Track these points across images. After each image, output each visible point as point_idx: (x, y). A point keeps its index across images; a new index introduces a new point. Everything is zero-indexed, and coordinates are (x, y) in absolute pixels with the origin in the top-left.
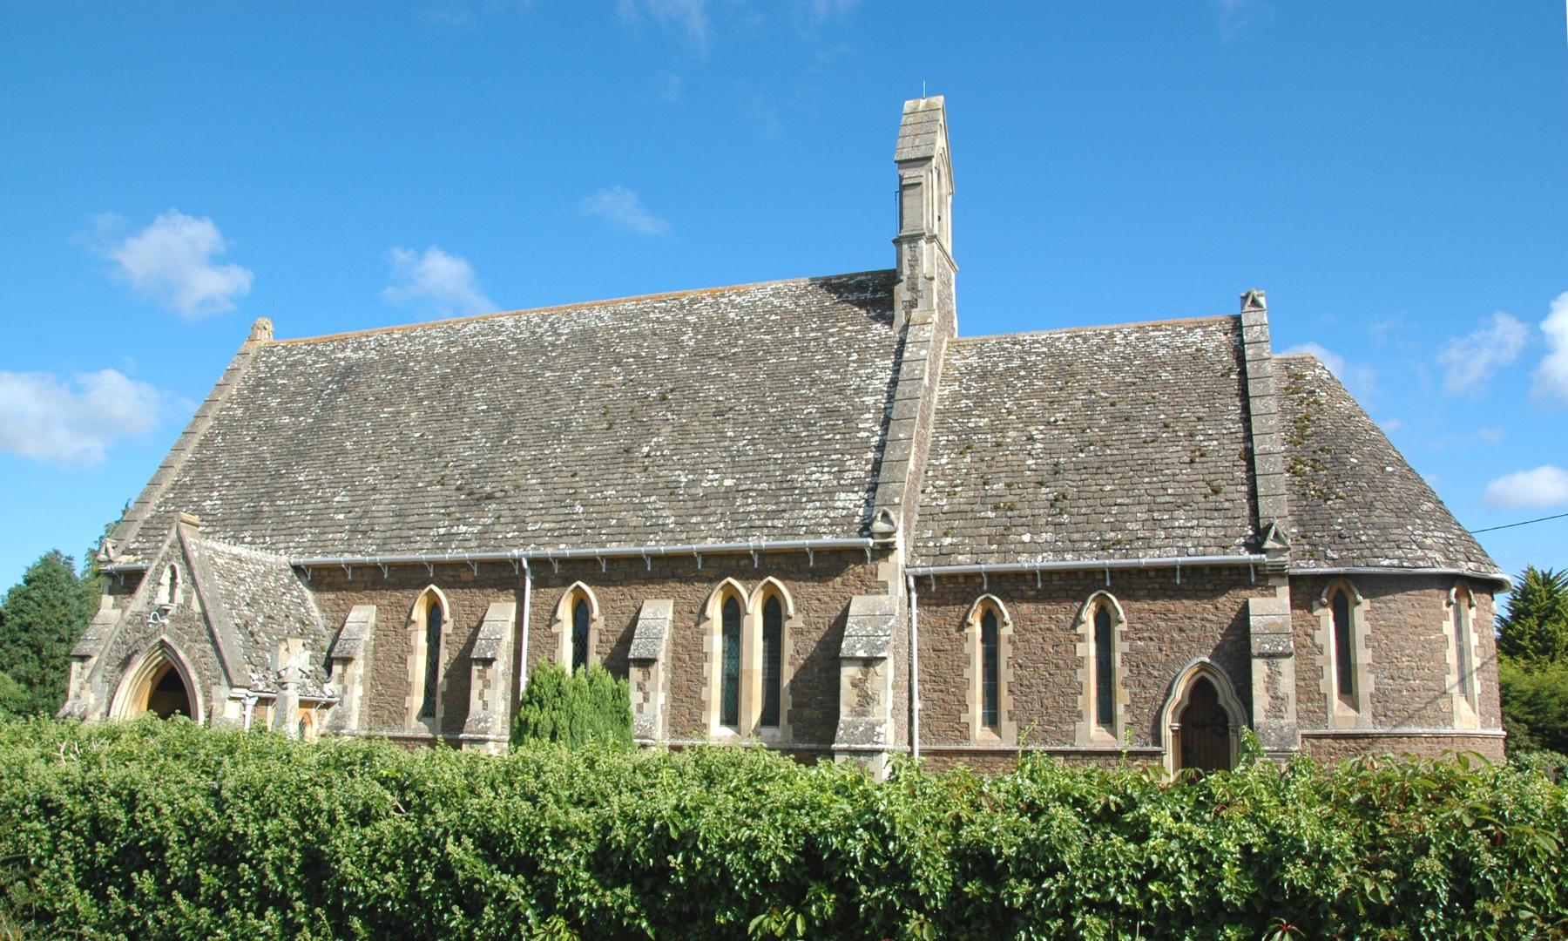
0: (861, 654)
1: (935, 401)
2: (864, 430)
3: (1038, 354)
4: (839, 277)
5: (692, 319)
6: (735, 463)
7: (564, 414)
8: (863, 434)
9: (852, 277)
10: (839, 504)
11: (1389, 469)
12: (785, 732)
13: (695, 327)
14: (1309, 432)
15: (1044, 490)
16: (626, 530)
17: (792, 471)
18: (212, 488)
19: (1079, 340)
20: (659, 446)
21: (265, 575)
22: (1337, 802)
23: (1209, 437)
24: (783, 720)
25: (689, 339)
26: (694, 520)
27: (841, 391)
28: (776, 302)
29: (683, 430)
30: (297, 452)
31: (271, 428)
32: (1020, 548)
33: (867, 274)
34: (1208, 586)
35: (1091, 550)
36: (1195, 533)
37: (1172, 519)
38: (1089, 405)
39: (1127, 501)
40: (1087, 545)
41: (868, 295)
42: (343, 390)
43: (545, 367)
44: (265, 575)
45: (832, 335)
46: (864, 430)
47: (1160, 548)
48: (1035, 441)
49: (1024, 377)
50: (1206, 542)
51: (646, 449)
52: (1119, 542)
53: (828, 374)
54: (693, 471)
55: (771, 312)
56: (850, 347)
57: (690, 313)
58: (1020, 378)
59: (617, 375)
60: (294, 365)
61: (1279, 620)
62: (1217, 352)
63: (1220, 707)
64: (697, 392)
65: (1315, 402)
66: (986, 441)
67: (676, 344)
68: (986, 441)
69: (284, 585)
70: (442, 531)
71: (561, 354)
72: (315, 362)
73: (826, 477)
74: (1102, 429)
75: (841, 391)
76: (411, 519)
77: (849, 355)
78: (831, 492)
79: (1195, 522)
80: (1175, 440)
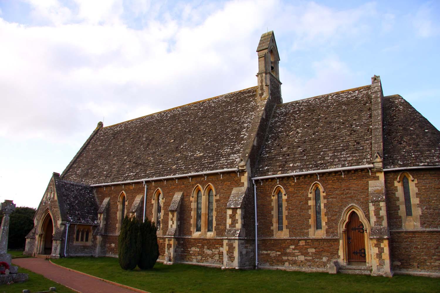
0: (232, 207)
1: (269, 124)
2: (242, 134)
3: (303, 106)
4: (244, 90)
5: (202, 108)
6: (205, 149)
7: (164, 139)
8: (242, 136)
9: (247, 89)
10: (231, 158)
11: (426, 131)
12: (214, 234)
13: (202, 110)
14: (395, 120)
15: (299, 149)
16: (171, 171)
17: (219, 149)
18: (80, 168)
19: (317, 100)
20: (186, 145)
21: (81, 190)
22: (182, 256)
23: (357, 126)
24: (214, 230)
25: (200, 114)
26: (190, 167)
27: (238, 123)
28: (225, 100)
29: (193, 140)
30: (100, 156)
31: (97, 150)
32: (288, 168)
33: (252, 88)
34: (354, 178)
35: (311, 168)
36: (349, 159)
37: (341, 154)
38: (318, 120)
39: (326, 150)
40: (311, 166)
41: (251, 94)
42: (114, 138)
43: (162, 126)
44: (81, 190)
45: (239, 107)
46: (242, 134)
47: (335, 165)
48: (299, 133)
49: (298, 113)
50: (352, 162)
51: (182, 147)
52: (322, 164)
53: (235, 119)
54: (192, 152)
55: (223, 103)
56: (243, 110)
57: (202, 106)
58: (297, 114)
59: (179, 126)
60: (105, 133)
61: (380, 188)
62: (362, 97)
63: (360, 222)
64: (199, 128)
65: (399, 110)
66: (283, 135)
67: (196, 116)
68: (283, 135)
69: (87, 193)
70: (127, 175)
71: (167, 122)
72: (110, 132)
73: (229, 150)
74: (321, 127)
75: (238, 123)
76: (121, 172)
77: (243, 112)
78: (229, 155)
79: (349, 155)
80: (345, 128)
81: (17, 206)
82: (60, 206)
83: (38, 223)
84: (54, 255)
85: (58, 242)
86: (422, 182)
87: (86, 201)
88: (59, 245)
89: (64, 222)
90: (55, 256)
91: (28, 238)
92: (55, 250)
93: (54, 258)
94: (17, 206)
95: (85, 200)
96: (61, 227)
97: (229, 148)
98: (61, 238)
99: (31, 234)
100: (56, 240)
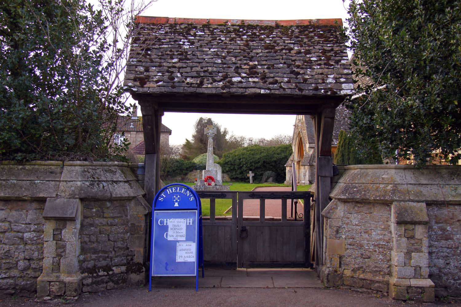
81: (191, 139)
82: (307, 128)
83: (295, 149)
84: (303, 182)
85: (306, 167)
86: (197, 67)
87: (344, 118)
88: (308, 170)
89: (311, 145)
90: (304, 183)
91: (287, 166)
92: (304, 176)
93: (303, 185)
94: (191, 139)
95: (342, 118)
96: (309, 151)
97: (197, 38)
98: (309, 163)
99: (289, 162)
100: (305, 165)
